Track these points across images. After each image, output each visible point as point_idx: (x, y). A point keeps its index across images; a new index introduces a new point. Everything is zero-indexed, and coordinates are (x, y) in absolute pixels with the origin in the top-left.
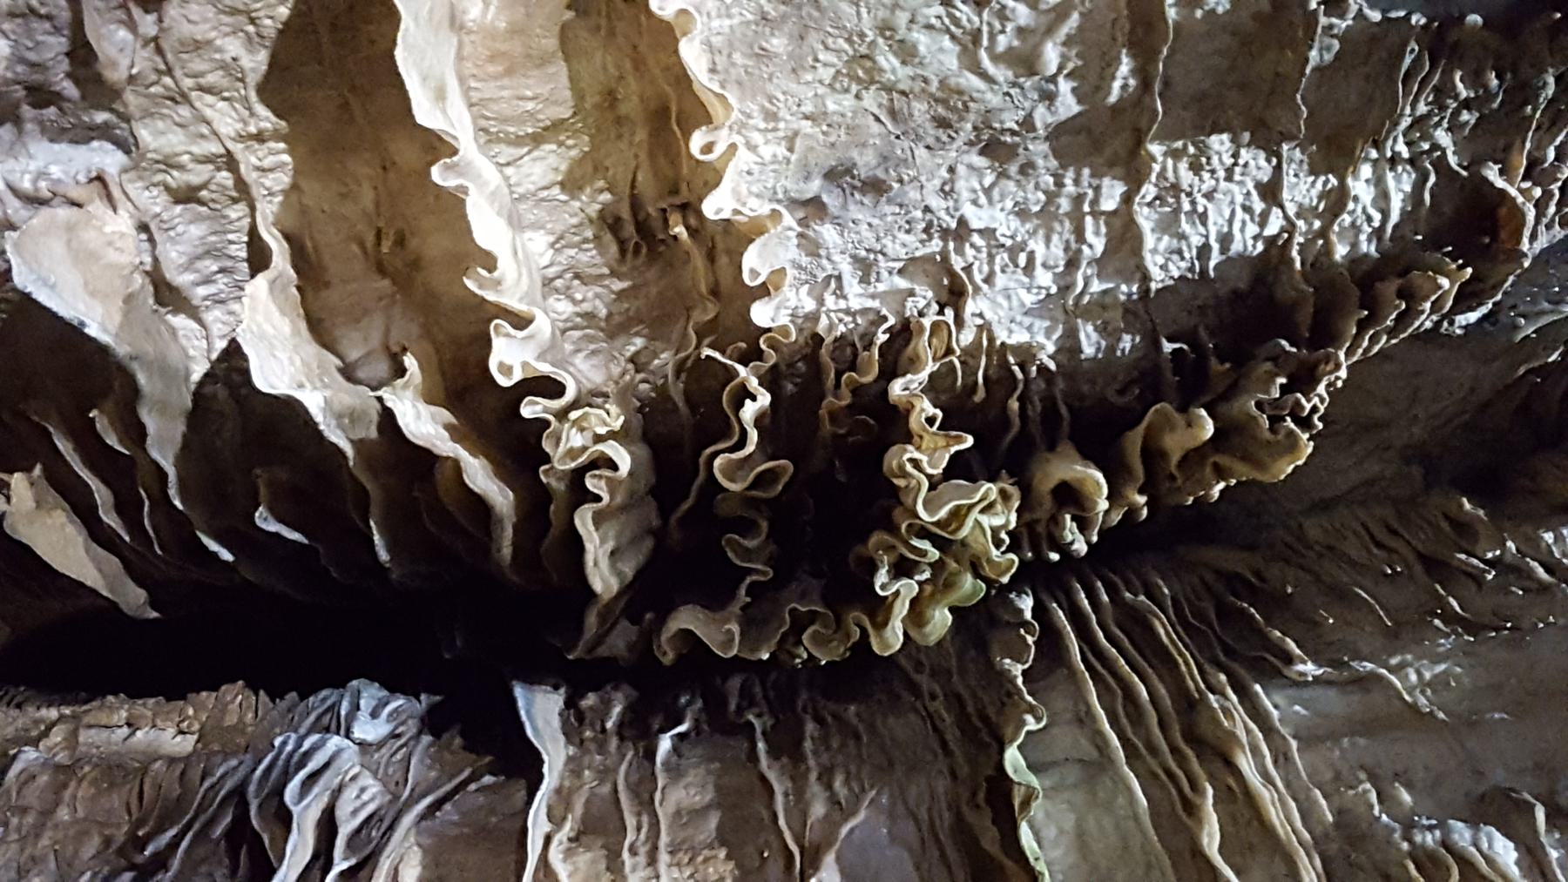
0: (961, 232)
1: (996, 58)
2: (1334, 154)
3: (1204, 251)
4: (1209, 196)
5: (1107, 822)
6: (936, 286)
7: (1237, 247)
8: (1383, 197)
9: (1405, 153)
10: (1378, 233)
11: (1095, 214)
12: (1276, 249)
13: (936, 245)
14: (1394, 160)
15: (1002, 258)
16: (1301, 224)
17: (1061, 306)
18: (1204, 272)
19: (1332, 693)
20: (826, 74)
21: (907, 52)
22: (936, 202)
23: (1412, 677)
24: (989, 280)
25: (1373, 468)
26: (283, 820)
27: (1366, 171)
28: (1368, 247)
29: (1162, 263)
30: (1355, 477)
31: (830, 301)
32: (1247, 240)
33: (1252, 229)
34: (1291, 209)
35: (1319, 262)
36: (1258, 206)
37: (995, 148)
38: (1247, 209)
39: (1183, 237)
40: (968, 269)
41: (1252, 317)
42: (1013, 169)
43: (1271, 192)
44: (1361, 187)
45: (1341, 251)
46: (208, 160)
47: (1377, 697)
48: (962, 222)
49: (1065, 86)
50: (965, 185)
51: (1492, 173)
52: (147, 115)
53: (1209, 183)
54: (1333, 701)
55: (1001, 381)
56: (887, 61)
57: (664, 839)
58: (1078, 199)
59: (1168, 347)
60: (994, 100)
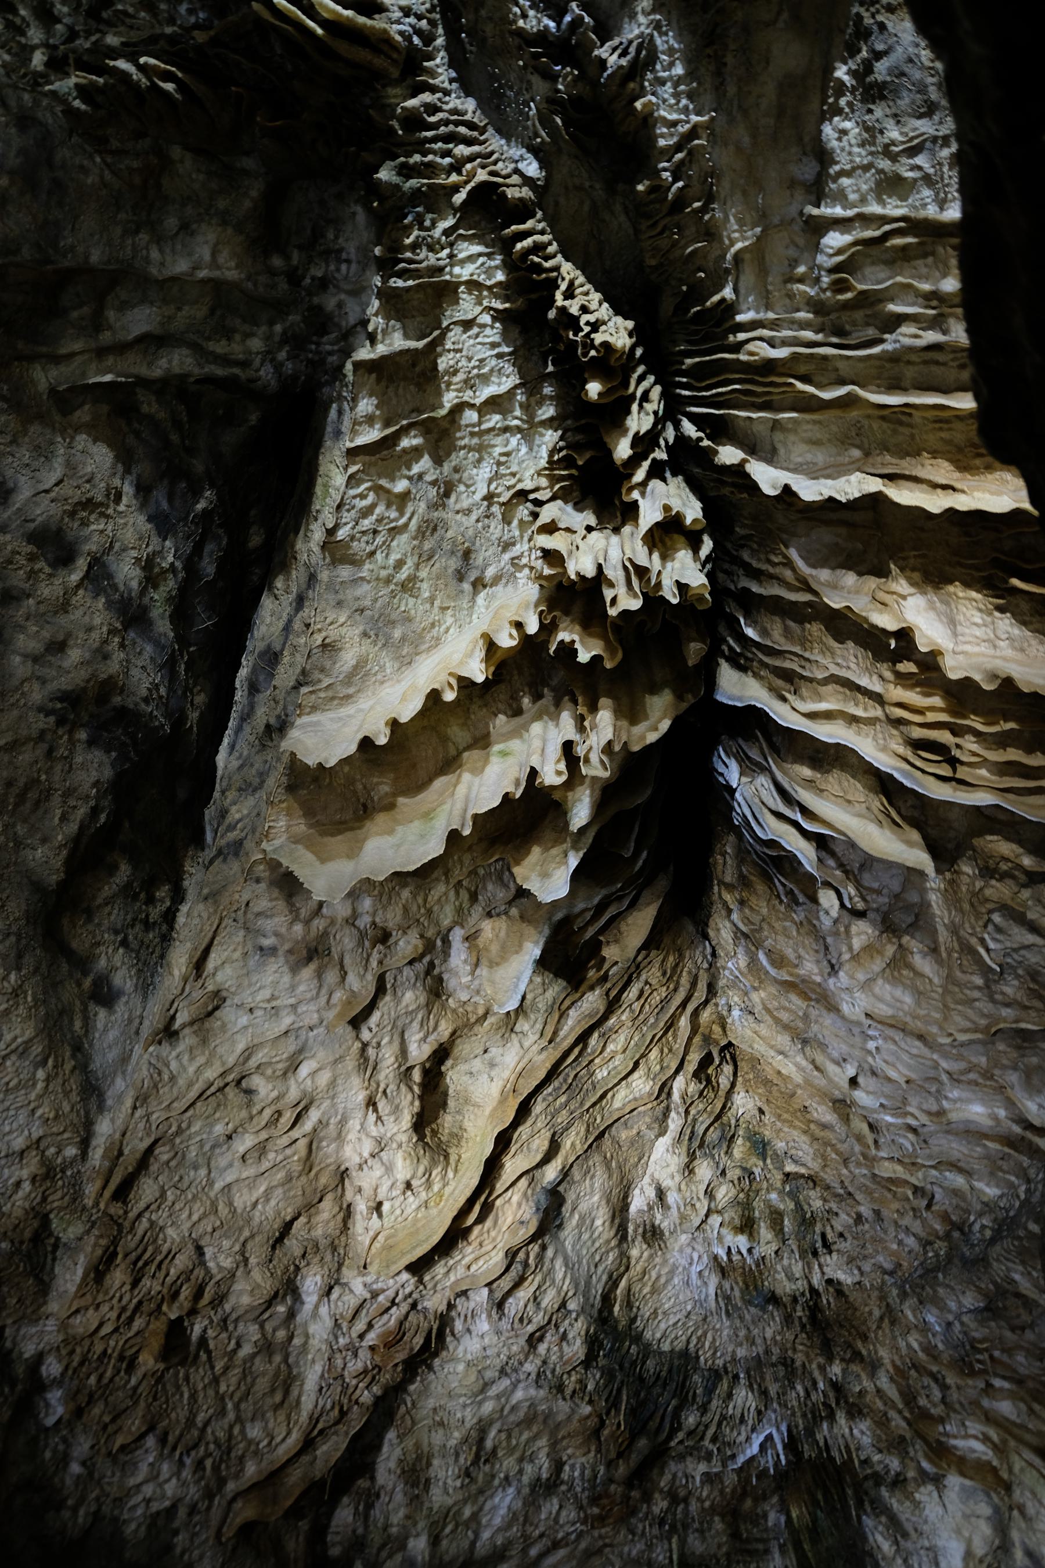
0: (489, 497)
1: (402, 514)
2: (446, 292)
3: (499, 356)
4: (470, 359)
5: (806, 427)
6: (518, 504)
7: (497, 339)
8: (471, 259)
9: (447, 251)
10: (489, 255)
11: (480, 423)
12: (499, 316)
13: (495, 509)
14: (451, 256)
15: (503, 470)
16: (485, 303)
17: (529, 432)
18: (510, 354)
19: (742, 278)
20: (411, 601)
21: (400, 564)
22: (474, 517)
23: (739, 240)
24: (514, 475)
25: (618, 208)
26: (773, 844)
27: (457, 270)
28: (498, 260)
29: (506, 382)
30: (622, 218)
31: (524, 561)
32: (493, 334)
33: (488, 331)
34: (479, 309)
35: (505, 290)
36: (475, 330)
37: (447, 489)
38: (477, 336)
39: (492, 370)
40: (509, 488)
41: (532, 323)
42: (457, 476)
43: (467, 325)
44: (464, 272)
45: (500, 276)
46: (457, 893)
47: (747, 256)
48: (484, 499)
49: (416, 469)
50: (465, 504)
51: (459, 198)
52: (437, 924)
53: (463, 362)
54: (748, 278)
55: (567, 462)
56: (403, 574)
57: (797, 649)
58: (472, 434)
59: (550, 368)
60: (423, 505)
